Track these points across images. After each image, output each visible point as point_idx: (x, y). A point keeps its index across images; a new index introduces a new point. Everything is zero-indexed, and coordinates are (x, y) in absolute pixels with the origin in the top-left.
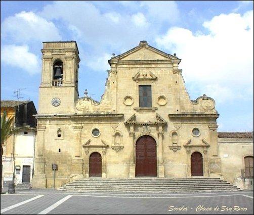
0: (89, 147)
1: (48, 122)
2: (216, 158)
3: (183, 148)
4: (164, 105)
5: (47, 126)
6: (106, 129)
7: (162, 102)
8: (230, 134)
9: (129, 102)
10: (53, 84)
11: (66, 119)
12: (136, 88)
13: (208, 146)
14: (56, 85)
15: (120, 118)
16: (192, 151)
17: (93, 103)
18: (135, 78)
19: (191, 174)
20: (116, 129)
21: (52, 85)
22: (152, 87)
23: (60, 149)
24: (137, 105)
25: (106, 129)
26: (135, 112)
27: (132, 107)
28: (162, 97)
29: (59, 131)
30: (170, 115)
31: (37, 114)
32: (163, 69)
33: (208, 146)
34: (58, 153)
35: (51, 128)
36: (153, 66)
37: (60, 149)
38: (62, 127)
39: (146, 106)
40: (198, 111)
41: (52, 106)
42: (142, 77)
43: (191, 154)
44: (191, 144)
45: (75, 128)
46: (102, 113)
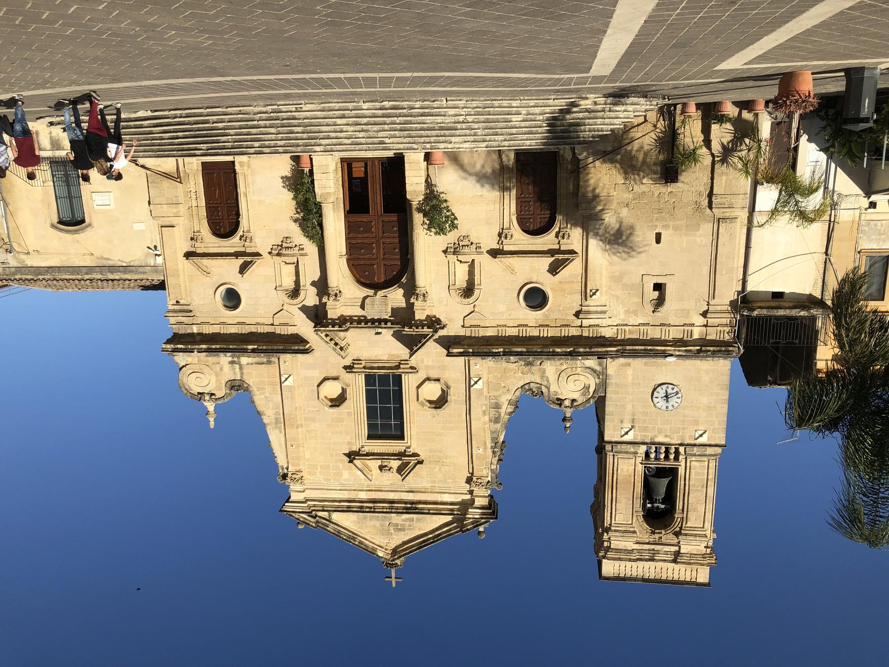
0: (551, 252)
1: (697, 334)
2: (167, 221)
3: (264, 251)
4: (325, 379)
5: (701, 321)
6: (502, 308)
7: (332, 390)
8: (90, 269)
9: (432, 391)
10: (677, 453)
11: (164, 157)
12: (410, 429)
13: (189, 255)
14: (667, 452)
15: (449, 344)
16: (235, 239)
17: (544, 390)
18: (413, 460)
19: (237, 167)
20: (470, 308)
21: (682, 449)
22: (365, 432)
23: (658, 241)
24: (409, 382)
25: (502, 308)
26: (413, 361)
27: (422, 375)
28: (338, 401)
29: (660, 302)
30: (306, 352)
31: (204, 164)
32: (334, 484)
33: (189, 255)
34: (666, 227)
35: (686, 312)
36: (363, 496)
37: (658, 241)
38: (645, 315)
39: (384, 379)
40: (225, 359)
41: (682, 385)
42: (395, 464)
43: (240, 233)
44: (240, 261)
45: (604, 312)
46: (512, 358)
